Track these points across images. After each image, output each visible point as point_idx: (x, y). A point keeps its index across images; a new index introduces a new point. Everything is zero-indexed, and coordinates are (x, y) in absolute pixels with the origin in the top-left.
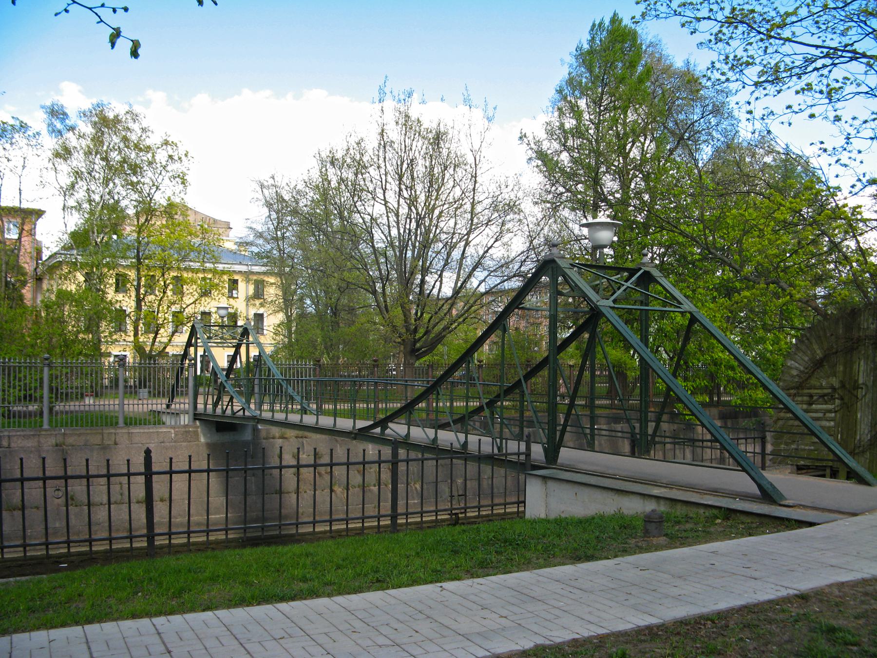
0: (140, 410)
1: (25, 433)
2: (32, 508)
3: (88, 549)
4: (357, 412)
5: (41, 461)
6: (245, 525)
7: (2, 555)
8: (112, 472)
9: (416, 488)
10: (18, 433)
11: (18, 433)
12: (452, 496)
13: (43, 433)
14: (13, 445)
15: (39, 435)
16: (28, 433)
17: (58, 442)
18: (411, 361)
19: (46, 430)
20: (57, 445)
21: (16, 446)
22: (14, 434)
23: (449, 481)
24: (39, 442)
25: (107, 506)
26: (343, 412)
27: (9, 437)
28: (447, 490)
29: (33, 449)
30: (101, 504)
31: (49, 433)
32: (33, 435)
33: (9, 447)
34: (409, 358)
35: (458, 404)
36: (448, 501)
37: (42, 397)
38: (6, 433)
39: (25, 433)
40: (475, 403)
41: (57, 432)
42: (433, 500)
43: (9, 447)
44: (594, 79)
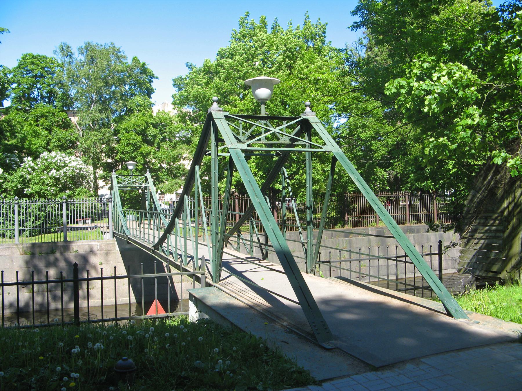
24: (12, 252)
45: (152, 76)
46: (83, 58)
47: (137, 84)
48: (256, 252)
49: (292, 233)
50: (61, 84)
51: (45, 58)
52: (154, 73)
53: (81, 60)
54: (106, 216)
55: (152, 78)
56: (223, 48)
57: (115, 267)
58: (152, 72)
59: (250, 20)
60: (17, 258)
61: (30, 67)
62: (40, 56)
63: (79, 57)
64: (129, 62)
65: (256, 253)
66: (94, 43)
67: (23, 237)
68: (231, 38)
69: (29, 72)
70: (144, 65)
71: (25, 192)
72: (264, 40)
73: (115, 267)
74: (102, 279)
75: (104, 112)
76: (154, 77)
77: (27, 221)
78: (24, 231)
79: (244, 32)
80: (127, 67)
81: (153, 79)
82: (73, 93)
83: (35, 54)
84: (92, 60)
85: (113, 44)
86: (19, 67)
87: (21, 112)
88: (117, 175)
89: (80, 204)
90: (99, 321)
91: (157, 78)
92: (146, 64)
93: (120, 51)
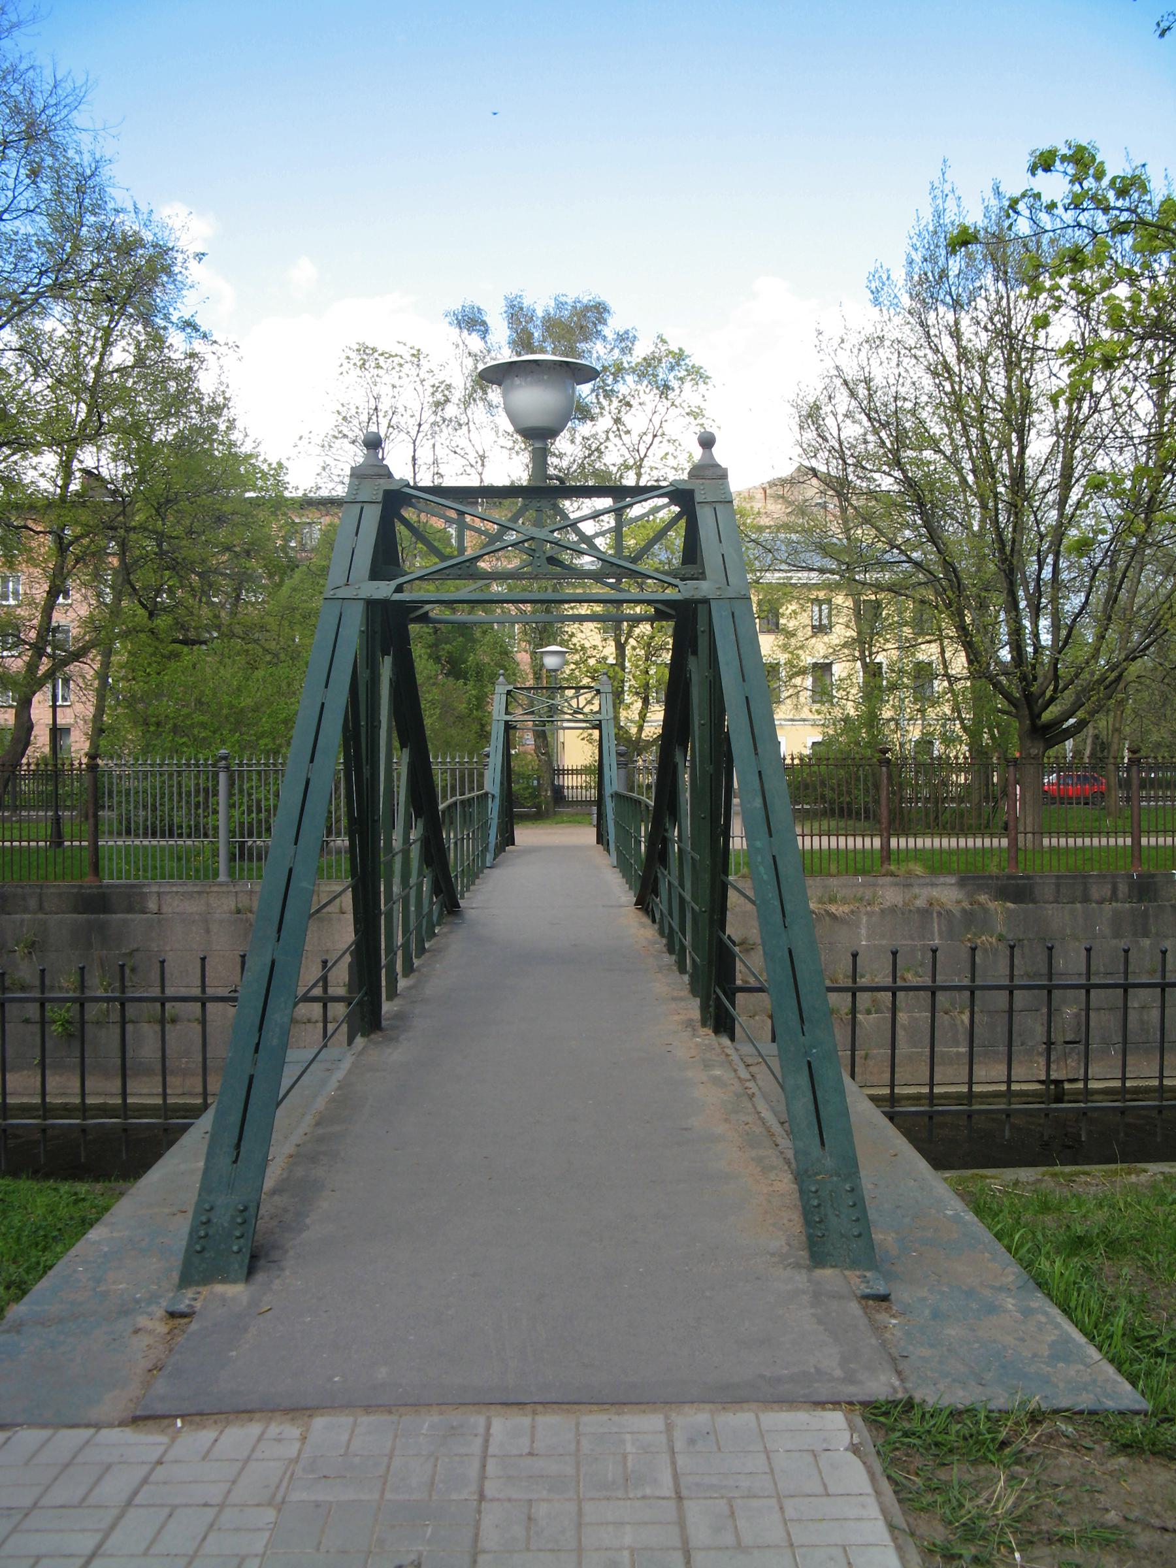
0: (808, 845)
1: (185, 889)
2: (189, 1021)
3: (161, 1102)
4: (1144, 854)
5: (1046, 952)
6: (970, 1104)
7: (4, 1099)
8: (979, 982)
9: (962, 1021)
10: (174, 889)
11: (174, 889)
12: (1049, 1044)
13: (215, 889)
14: (165, 909)
15: (208, 893)
16: (191, 889)
17: (240, 906)
18: (1034, 751)
19: (221, 885)
20: (238, 912)
21: (170, 910)
22: (167, 889)
23: (1045, 1010)
24: (208, 905)
25: (321, 1025)
26: (912, 854)
27: (159, 894)
28: (1040, 1031)
29: (197, 917)
30: (309, 1021)
31: (224, 889)
32: (199, 893)
33: (159, 913)
34: (1028, 744)
35: (1153, 841)
36: (1040, 1054)
37: (216, 828)
38: (155, 889)
39: (185, 889)
40: (1120, 841)
41: (238, 889)
42: (1003, 1049)
43: (159, 913)
44: (1159, 212)
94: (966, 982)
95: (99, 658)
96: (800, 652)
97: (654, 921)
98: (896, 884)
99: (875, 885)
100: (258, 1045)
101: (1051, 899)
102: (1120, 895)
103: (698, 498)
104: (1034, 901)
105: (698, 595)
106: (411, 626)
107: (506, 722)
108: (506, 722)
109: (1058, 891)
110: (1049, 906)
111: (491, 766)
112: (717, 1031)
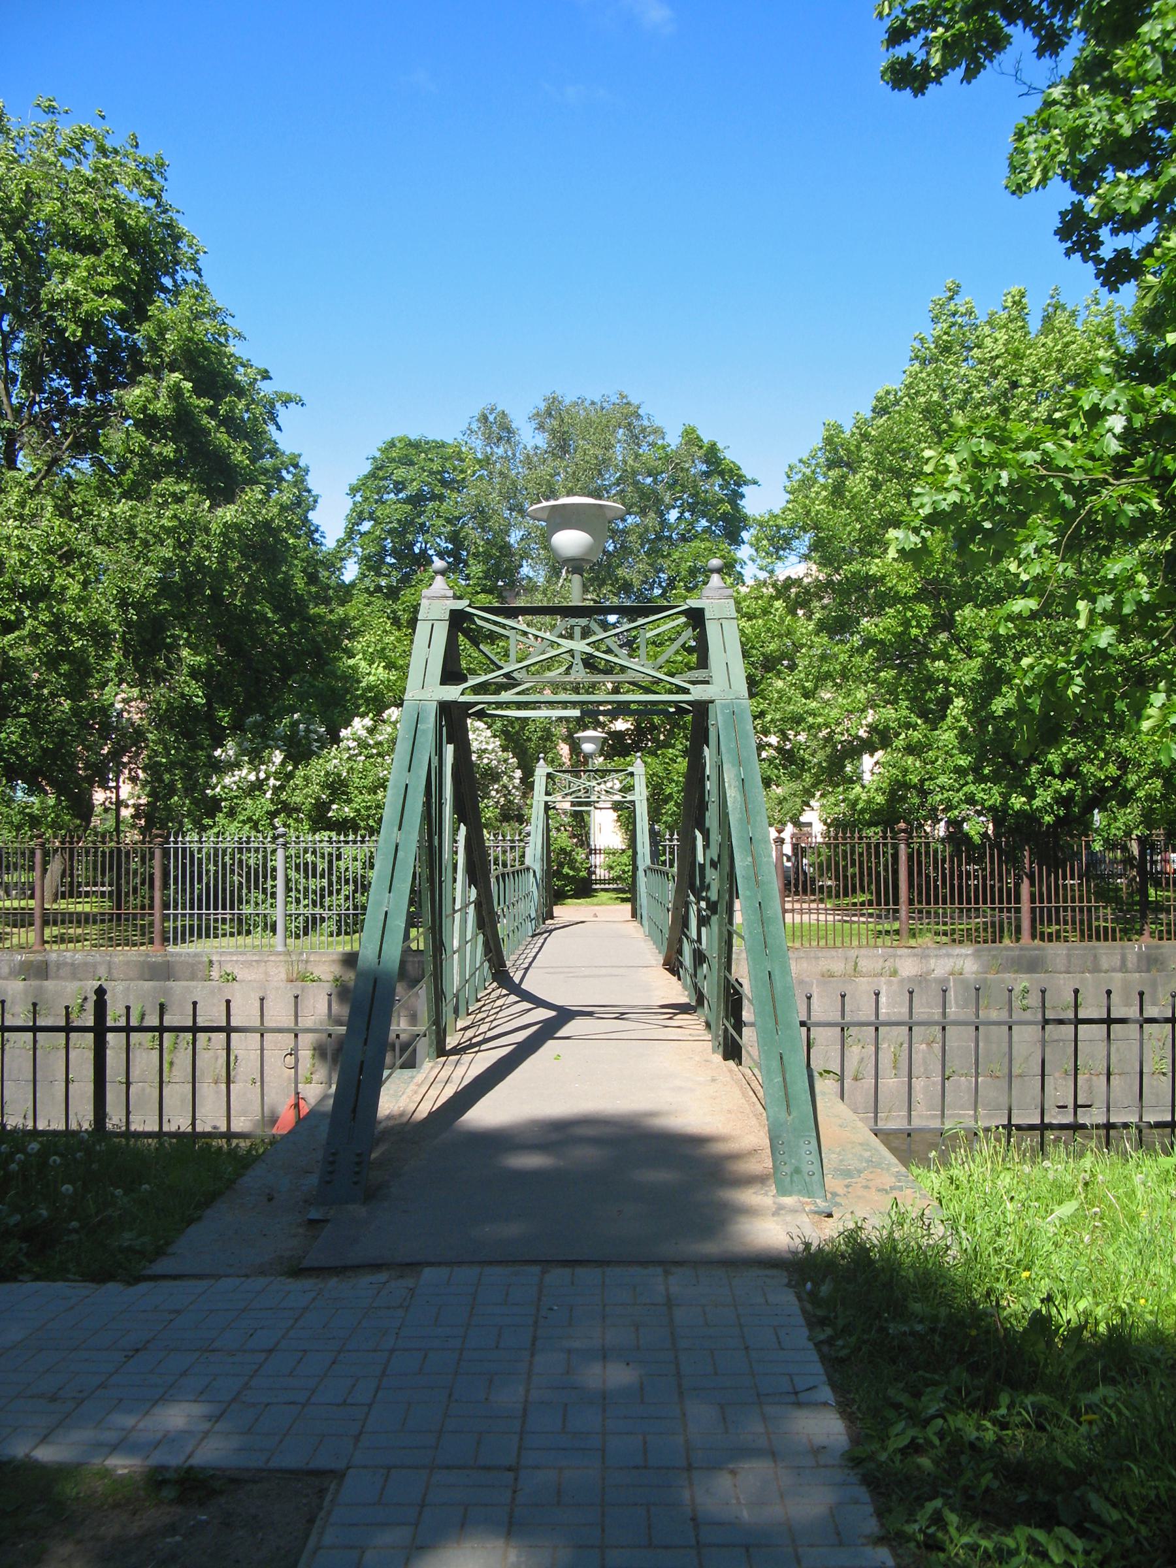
10: (235, 958)
11: (235, 958)
13: (272, 958)
24: (266, 973)
45: (741, 481)
46: (541, 440)
47: (698, 506)
48: (956, 1002)
49: (1075, 948)
50: (481, 514)
51: (443, 445)
52: (744, 472)
53: (537, 448)
54: (800, 889)
55: (739, 486)
56: (889, 388)
57: (228, 1002)
58: (739, 468)
59: (960, 303)
60: (277, 989)
61: (400, 473)
62: (427, 443)
63: (531, 439)
64: (673, 440)
65: (958, 1006)
66: (567, 401)
67: (322, 935)
68: (911, 360)
69: (399, 487)
70: (713, 448)
71: (330, 814)
72: (997, 357)
73: (228, 1002)
74: (195, 1029)
75: (595, 590)
76: (746, 483)
77: (331, 894)
78: (323, 920)
79: (945, 337)
80: (668, 459)
81: (744, 490)
82: (514, 537)
83: (414, 436)
84: (562, 445)
85: (626, 397)
86: (373, 475)
87: (379, 598)
88: (550, 770)
89: (240, 850)
90: (222, 1135)
91: (755, 483)
92: (720, 446)
93: (638, 416)
94: (937, 1017)
95: (474, 757)
96: (273, 808)
97: (679, 979)
98: (915, 955)
99: (895, 956)
100: (366, 1040)
101: (1063, 969)
102: (1129, 965)
103: (707, 615)
104: (1046, 972)
105: (705, 697)
106: (469, 721)
107: (546, 803)
108: (546, 803)
109: (1069, 962)
110: (1062, 976)
111: (531, 844)
112: (726, 1058)
